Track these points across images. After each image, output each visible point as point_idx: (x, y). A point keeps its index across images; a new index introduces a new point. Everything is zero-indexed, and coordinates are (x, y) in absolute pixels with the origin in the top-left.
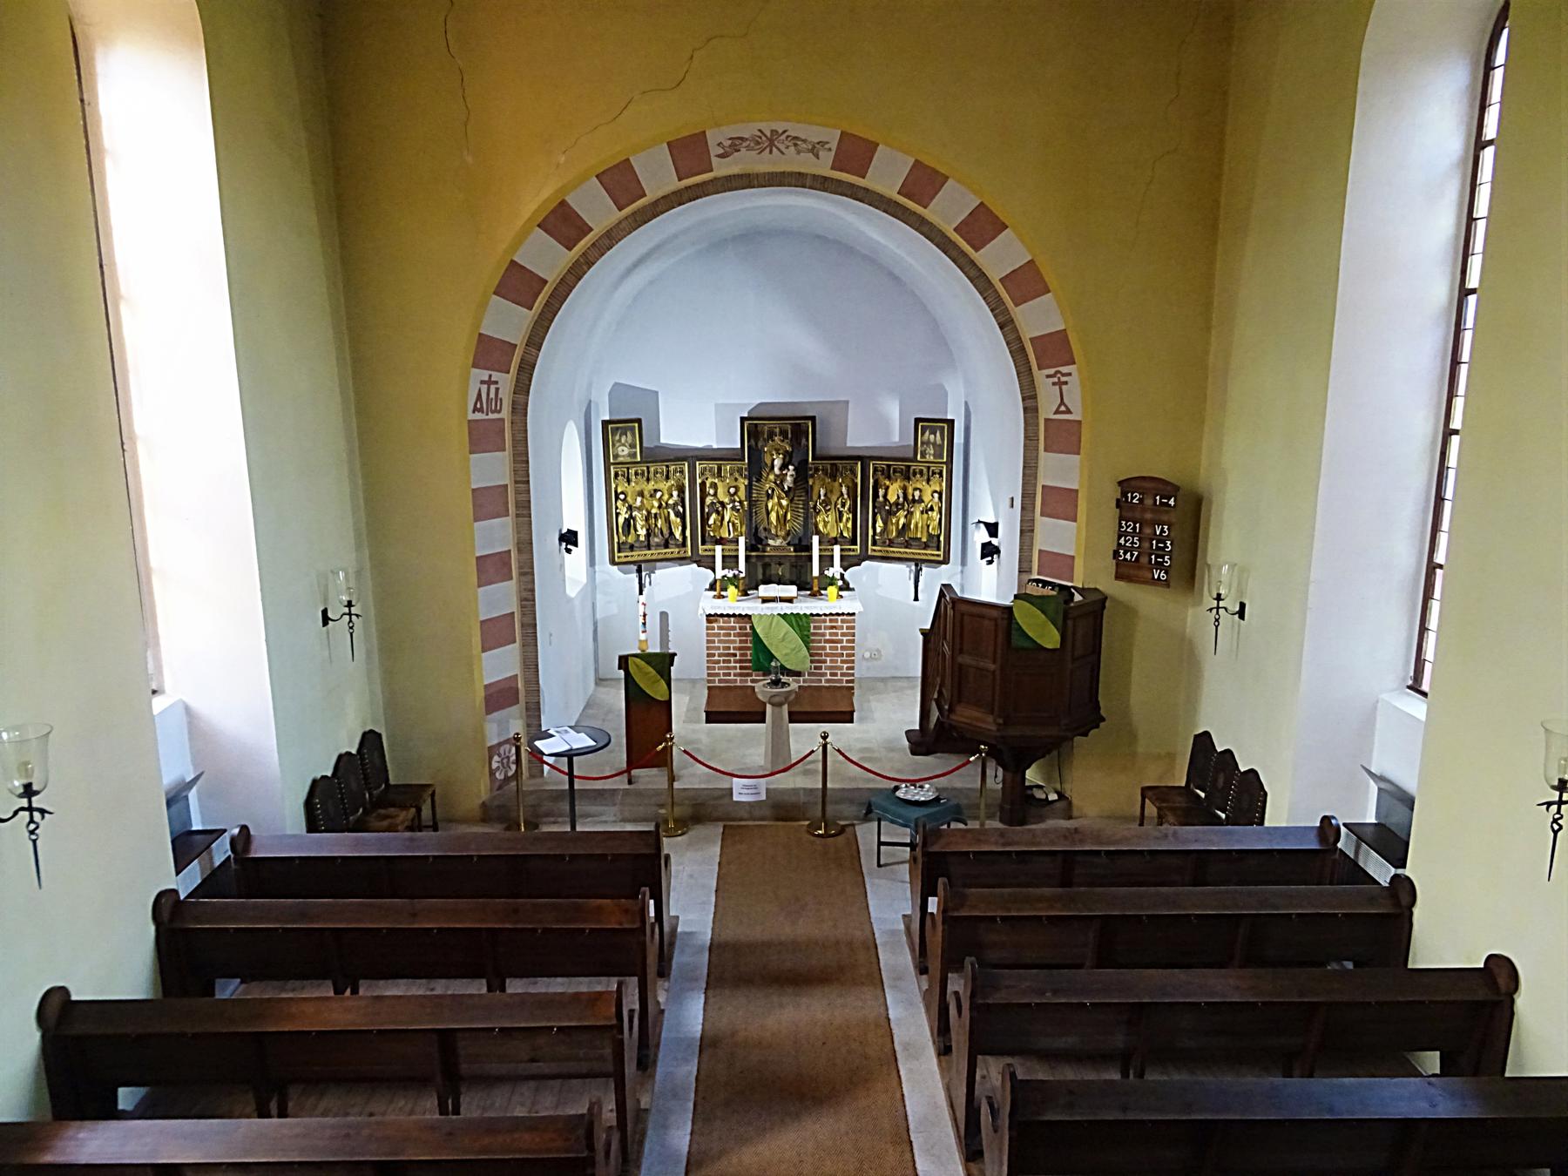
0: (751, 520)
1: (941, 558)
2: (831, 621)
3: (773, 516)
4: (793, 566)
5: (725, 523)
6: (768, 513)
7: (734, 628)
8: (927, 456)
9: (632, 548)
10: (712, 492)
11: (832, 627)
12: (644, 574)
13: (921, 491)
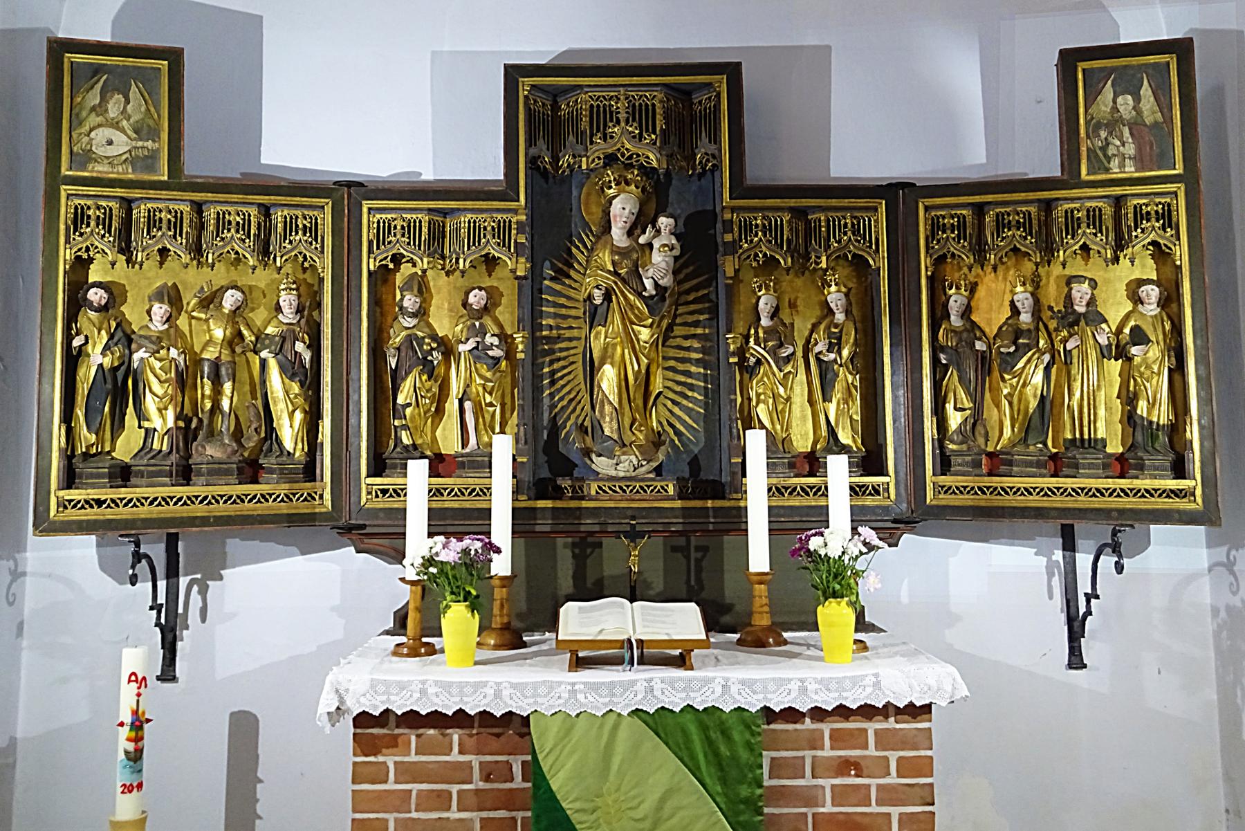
0: (536, 402)
1: (1198, 504)
2: (838, 739)
3: (608, 378)
4: (675, 549)
5: (452, 406)
6: (592, 370)
7: (460, 773)
8: (1115, 164)
9: (123, 474)
10: (410, 302)
11: (845, 766)
12: (183, 581)
13: (1094, 284)
